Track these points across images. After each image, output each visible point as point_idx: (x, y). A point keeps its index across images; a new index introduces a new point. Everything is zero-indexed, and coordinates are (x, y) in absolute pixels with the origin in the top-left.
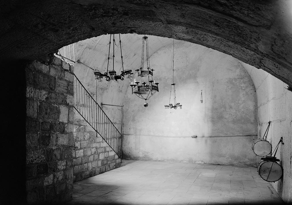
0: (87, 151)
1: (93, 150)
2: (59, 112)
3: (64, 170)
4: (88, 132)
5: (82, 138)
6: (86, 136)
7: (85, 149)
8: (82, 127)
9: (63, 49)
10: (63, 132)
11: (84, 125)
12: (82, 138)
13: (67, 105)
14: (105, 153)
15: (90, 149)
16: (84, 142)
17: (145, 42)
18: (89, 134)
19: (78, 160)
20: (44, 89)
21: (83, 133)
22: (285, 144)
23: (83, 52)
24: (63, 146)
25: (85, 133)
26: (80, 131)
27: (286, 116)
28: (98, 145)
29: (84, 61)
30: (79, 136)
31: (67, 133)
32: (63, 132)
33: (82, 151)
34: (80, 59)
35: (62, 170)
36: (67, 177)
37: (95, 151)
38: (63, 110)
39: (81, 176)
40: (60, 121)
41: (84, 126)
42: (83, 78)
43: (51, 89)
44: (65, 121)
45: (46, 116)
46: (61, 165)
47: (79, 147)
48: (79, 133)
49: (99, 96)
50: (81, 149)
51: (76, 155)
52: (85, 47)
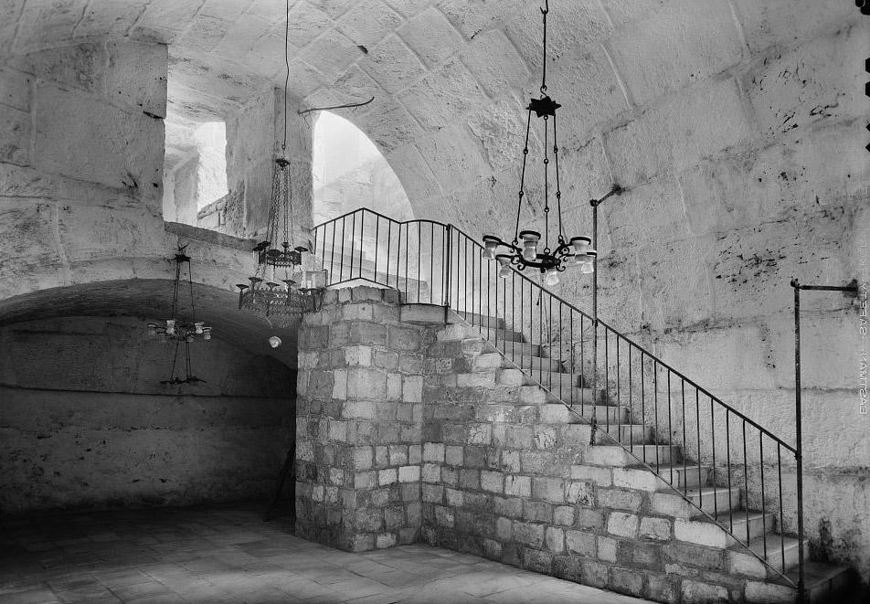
1: (575, 491)
2: (332, 383)
3: (340, 487)
6: (542, 437)
7: (537, 479)
8: (527, 407)
9: (317, 283)
12: (526, 443)
15: (558, 481)
16: (533, 455)
18: (552, 433)
19: (510, 502)
21: (531, 427)
23: (608, 154)
24: (338, 442)
25: (538, 429)
27: (824, 66)
28: (600, 478)
29: (637, 174)
30: (514, 434)
32: (339, 417)
33: (525, 481)
35: (337, 486)
36: (344, 503)
37: (583, 494)
38: (339, 376)
41: (535, 405)
46: (337, 476)
47: (517, 469)
48: (515, 427)
49: (817, 257)
50: (522, 473)
52: (599, 138)
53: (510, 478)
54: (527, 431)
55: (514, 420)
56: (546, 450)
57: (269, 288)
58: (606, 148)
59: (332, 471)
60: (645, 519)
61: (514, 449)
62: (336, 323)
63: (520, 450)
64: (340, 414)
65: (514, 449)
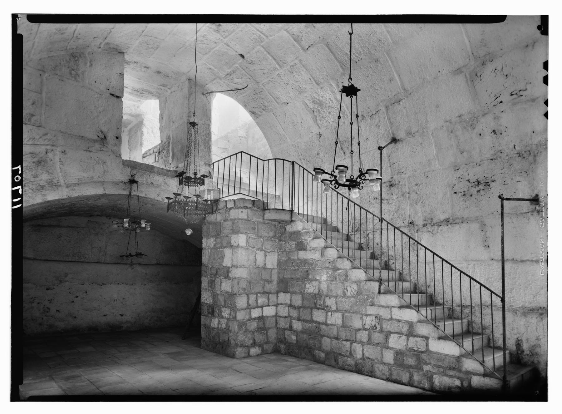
0: (351, 319)
1: (369, 322)
2: (223, 257)
3: (228, 319)
4: (355, 282)
5: (340, 292)
6: (349, 289)
7: (346, 314)
8: (340, 271)
10: (227, 277)
11: (345, 268)
12: (340, 292)
13: (232, 246)
14: (411, 339)
16: (344, 300)
17: (193, 132)
18: (355, 287)
19: (330, 328)
20: (213, 237)
21: (343, 283)
22: (376, 147)
24: (227, 292)
25: (347, 284)
26: (336, 279)
28: (384, 313)
31: (230, 279)
32: (227, 277)
33: (338, 315)
34: (393, 134)
38: (227, 252)
39: (336, 361)
40: (224, 265)
42: (430, 163)
43: (218, 235)
44: (229, 265)
45: (214, 262)
46: (226, 313)
47: (334, 308)
50: (337, 311)
51: (328, 320)
52: (384, 109)
54: (340, 285)
56: (352, 297)
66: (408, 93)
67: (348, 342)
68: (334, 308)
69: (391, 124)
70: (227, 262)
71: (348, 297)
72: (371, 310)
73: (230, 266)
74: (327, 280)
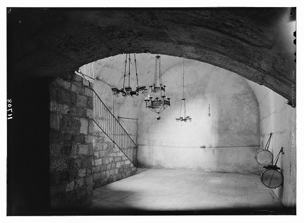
2: (79, 125)
3: (84, 177)
6: (104, 146)
8: (101, 138)
9: (84, 67)
11: (103, 136)
13: (87, 118)
15: (108, 158)
16: (102, 152)
18: (106, 145)
20: (66, 103)
24: (83, 155)
25: (104, 144)
28: (115, 155)
31: (87, 144)
32: (83, 142)
33: (100, 160)
34: (99, 76)
35: (83, 177)
38: (84, 123)
39: (100, 183)
40: (81, 132)
41: (103, 137)
44: (86, 133)
46: (82, 173)
47: (98, 157)
50: (99, 158)
52: (103, 65)
53: (96, 160)
54: (101, 145)
55: (97, 141)
56: (105, 150)
57: (157, 100)
58: (102, 68)
59: (80, 171)
60: (122, 162)
61: (98, 151)
62: (81, 94)
63: (99, 151)
64: (84, 141)
65: (98, 151)
66: (112, 68)
67: (104, 172)
68: (98, 157)
69: (101, 72)
70: (83, 130)
71: (104, 150)
72: (112, 155)
73: (86, 134)
74: (95, 142)
